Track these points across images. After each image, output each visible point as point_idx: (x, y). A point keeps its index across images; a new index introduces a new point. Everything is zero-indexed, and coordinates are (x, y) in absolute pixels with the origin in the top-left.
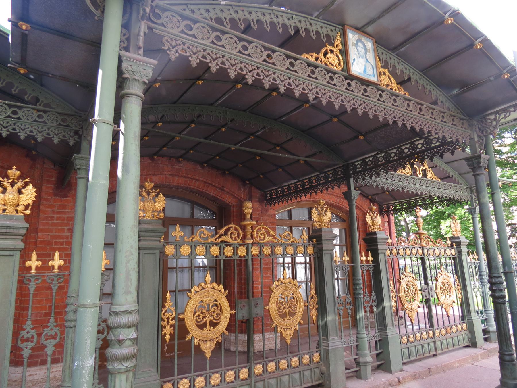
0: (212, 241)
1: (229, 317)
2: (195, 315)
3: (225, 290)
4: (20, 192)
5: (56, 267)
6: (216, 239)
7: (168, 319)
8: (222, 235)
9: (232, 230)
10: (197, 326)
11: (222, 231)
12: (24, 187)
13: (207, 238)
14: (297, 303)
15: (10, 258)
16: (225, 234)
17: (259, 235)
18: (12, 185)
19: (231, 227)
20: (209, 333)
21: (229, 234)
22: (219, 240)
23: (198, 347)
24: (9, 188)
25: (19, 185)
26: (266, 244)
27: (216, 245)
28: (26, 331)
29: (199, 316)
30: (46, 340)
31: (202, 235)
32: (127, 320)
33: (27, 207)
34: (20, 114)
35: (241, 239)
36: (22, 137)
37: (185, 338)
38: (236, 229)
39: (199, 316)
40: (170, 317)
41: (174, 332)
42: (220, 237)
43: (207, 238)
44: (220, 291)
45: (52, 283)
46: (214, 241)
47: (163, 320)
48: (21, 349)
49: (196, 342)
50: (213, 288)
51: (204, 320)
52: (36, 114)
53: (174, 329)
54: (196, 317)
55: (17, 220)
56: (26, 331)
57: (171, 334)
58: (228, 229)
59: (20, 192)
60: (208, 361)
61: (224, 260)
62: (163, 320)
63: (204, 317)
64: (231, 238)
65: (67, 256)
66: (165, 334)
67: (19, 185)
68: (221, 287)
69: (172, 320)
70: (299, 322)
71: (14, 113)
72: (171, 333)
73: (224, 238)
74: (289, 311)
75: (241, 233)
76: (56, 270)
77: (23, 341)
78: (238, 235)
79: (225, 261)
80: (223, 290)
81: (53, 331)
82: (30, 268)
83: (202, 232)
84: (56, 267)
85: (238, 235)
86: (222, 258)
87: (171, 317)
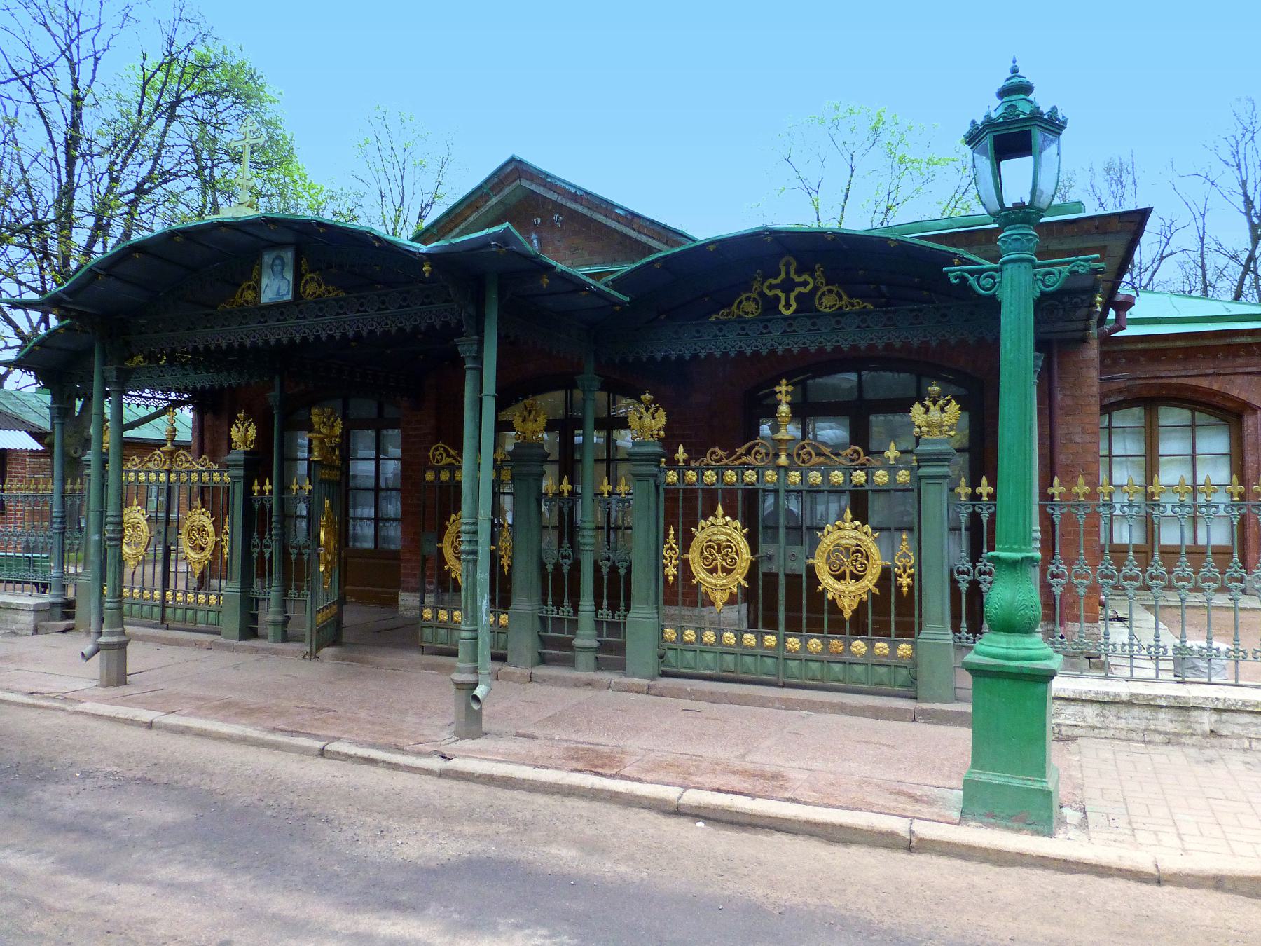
4: (942, 411)
10: (834, 577)
13: (720, 460)
16: (748, 453)
20: (849, 586)
22: (737, 463)
23: (833, 603)
24: (932, 408)
26: (444, 468)
32: (585, 541)
33: (951, 427)
34: (770, 329)
36: (829, 350)
42: (739, 457)
43: (720, 460)
48: (1051, 586)
50: (856, 528)
52: (809, 322)
55: (652, 444)
57: (908, 586)
58: (752, 447)
59: (942, 411)
60: (848, 625)
65: (993, 483)
67: (941, 402)
68: (738, 524)
71: (889, 319)
73: (744, 459)
79: (744, 490)
80: (739, 526)
83: (714, 452)
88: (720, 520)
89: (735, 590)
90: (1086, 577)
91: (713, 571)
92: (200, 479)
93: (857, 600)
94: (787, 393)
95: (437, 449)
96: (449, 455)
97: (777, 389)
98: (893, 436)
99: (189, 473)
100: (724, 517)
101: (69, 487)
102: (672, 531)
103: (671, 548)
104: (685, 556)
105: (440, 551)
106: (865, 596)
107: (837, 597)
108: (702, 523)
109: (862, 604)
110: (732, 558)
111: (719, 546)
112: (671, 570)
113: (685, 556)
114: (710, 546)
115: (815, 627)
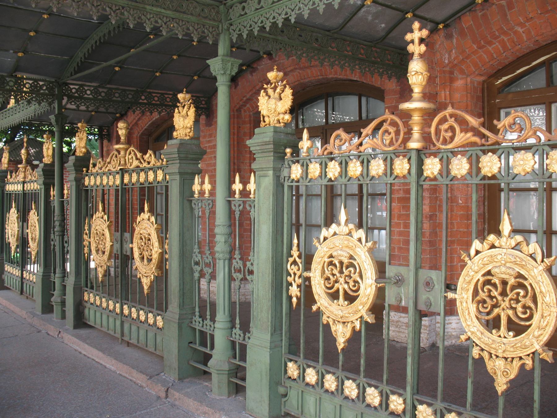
9: (385, 126)
17: (443, 133)
44: (532, 257)
60: (501, 402)
88: (344, 229)
89: (529, 362)
91: (493, 324)
92: (323, 173)
93: (517, 364)
94: (422, 41)
95: (444, 120)
96: (465, 127)
97: (408, 37)
98: (6, 149)
99: (365, 162)
100: (346, 223)
101: (237, 186)
102: (295, 241)
103: (295, 263)
104: (306, 274)
105: (132, 249)
106: (529, 362)
107: (486, 355)
108: (476, 245)
109: (355, 334)
110: (356, 282)
111: (341, 263)
112: (294, 291)
113: (306, 274)
114: (488, 282)
115: (312, 356)
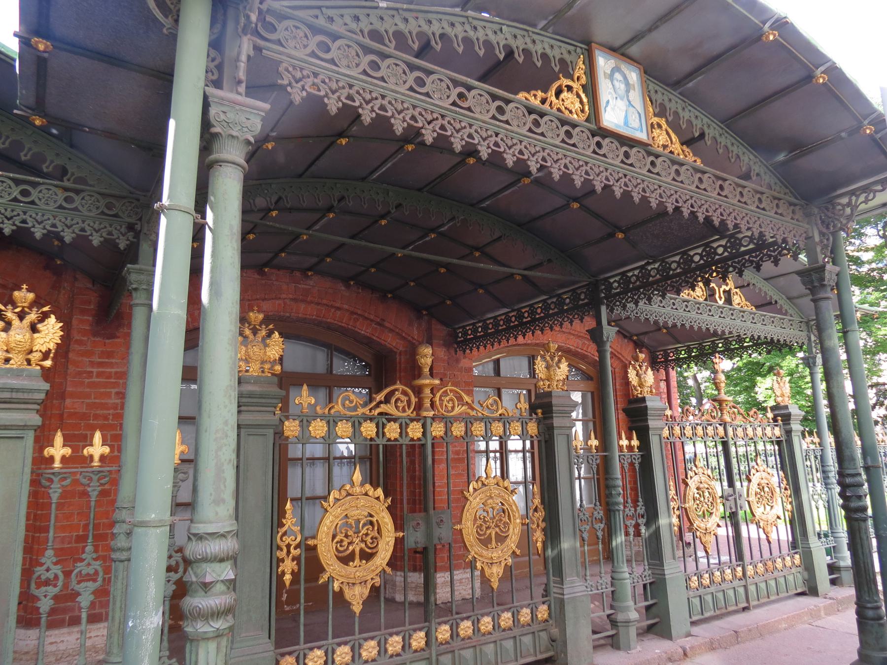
0: (363, 413)
1: (392, 543)
2: (335, 541)
3: (386, 496)
4: (34, 329)
5: (96, 458)
6: (370, 410)
7: (288, 546)
8: (381, 402)
9: (398, 395)
10: (339, 558)
11: (380, 397)
12: (42, 320)
13: (355, 408)
14: (509, 519)
15: (18, 441)
16: (387, 400)
17: (445, 403)
18: (21, 316)
19: (396, 390)
20: (358, 570)
21: (393, 400)
22: (376, 412)
23: (339, 596)
24: (16, 322)
25: (33, 316)
26: (456, 419)
27: (371, 420)
28: (45, 567)
29: (342, 541)
30: (79, 582)
31: (347, 402)
32: (217, 548)
33: (46, 355)
34: (34, 195)
35: (414, 409)
36: (38, 235)
37: (317, 579)
38: (405, 393)
39: (342, 541)
40: (291, 543)
41: (299, 569)
42: (378, 405)
43: (355, 408)
44: (378, 498)
45: (88, 485)
46: (368, 413)
47: (279, 548)
48: (36, 599)
49: (336, 586)
50: (366, 494)
51: (351, 548)
52: (61, 195)
53: (299, 564)
54: (337, 543)
55: (30, 376)
56: (45, 567)
57: (293, 573)
58: (392, 393)
59: (34, 329)
60: (357, 619)
61: (385, 446)
62: (279, 548)
63: (349, 544)
64: (397, 407)
65: (115, 440)
66: (283, 573)
67: (33, 316)
68: (380, 492)
69: (295, 548)
70: (514, 552)
71: (25, 193)
72: (293, 571)
73: (384, 408)
74: (496, 533)
75: (414, 400)
76: (96, 463)
77: (39, 585)
78: (409, 402)
79: (385, 447)
80: (382, 497)
81: (91, 567)
82: (51, 459)
83: (347, 398)
84: (96, 458)
85: (409, 402)
86: (381, 442)
87: (294, 544)
90: (92, 578)
